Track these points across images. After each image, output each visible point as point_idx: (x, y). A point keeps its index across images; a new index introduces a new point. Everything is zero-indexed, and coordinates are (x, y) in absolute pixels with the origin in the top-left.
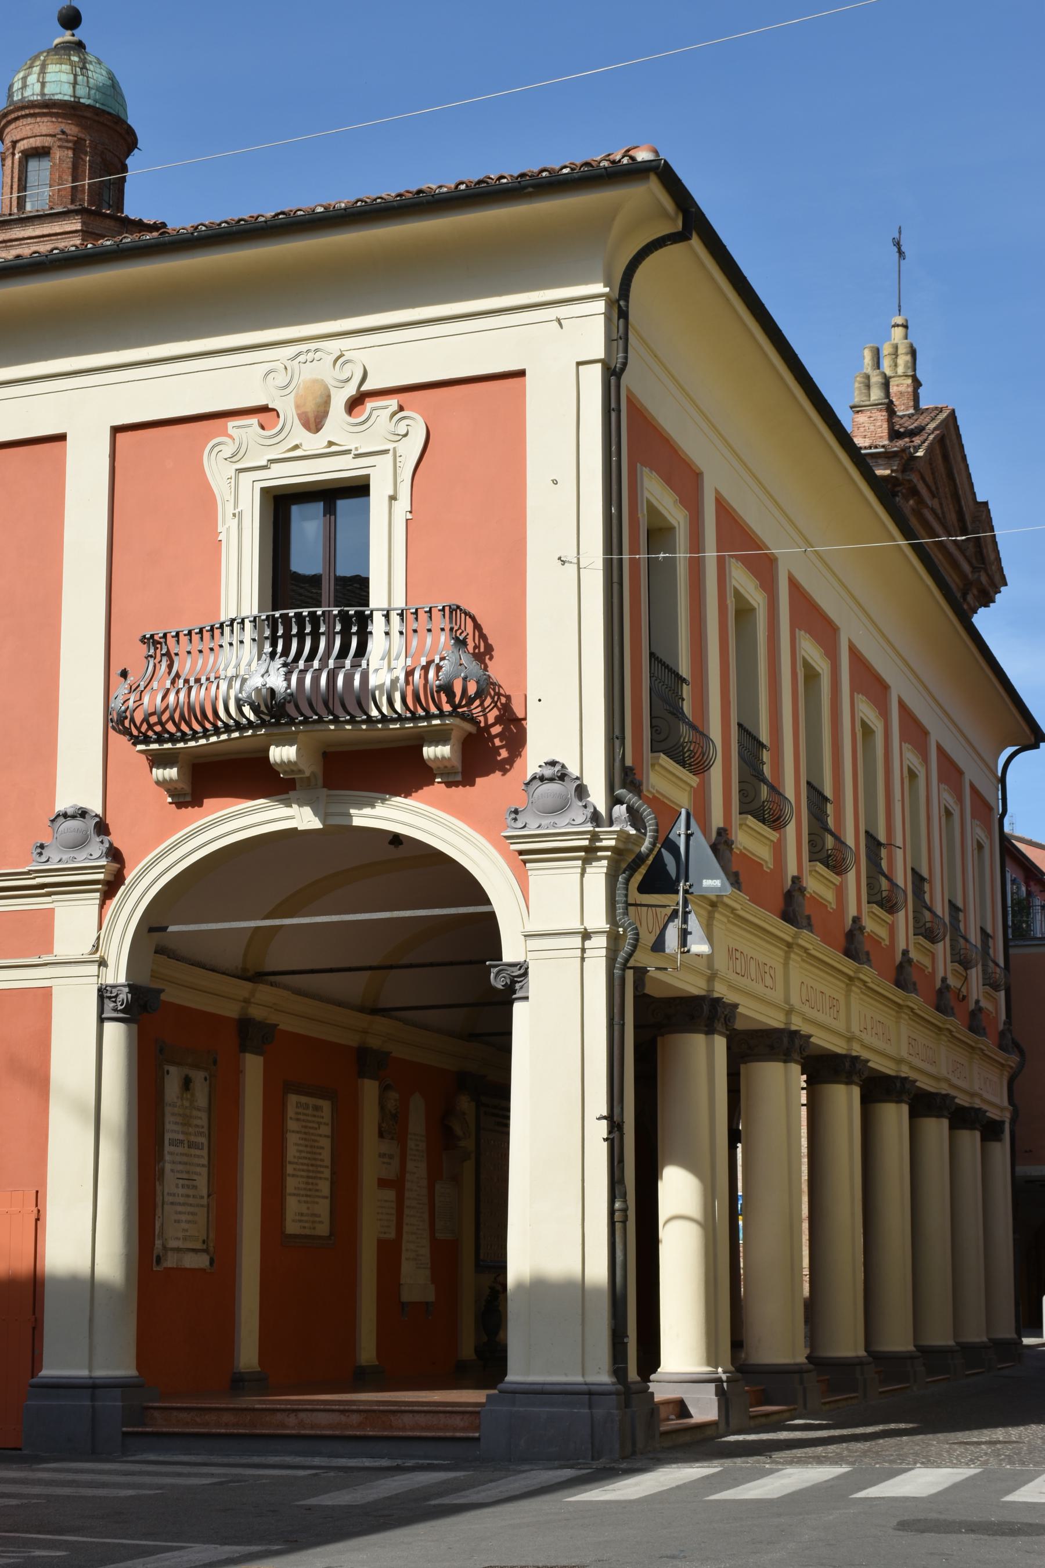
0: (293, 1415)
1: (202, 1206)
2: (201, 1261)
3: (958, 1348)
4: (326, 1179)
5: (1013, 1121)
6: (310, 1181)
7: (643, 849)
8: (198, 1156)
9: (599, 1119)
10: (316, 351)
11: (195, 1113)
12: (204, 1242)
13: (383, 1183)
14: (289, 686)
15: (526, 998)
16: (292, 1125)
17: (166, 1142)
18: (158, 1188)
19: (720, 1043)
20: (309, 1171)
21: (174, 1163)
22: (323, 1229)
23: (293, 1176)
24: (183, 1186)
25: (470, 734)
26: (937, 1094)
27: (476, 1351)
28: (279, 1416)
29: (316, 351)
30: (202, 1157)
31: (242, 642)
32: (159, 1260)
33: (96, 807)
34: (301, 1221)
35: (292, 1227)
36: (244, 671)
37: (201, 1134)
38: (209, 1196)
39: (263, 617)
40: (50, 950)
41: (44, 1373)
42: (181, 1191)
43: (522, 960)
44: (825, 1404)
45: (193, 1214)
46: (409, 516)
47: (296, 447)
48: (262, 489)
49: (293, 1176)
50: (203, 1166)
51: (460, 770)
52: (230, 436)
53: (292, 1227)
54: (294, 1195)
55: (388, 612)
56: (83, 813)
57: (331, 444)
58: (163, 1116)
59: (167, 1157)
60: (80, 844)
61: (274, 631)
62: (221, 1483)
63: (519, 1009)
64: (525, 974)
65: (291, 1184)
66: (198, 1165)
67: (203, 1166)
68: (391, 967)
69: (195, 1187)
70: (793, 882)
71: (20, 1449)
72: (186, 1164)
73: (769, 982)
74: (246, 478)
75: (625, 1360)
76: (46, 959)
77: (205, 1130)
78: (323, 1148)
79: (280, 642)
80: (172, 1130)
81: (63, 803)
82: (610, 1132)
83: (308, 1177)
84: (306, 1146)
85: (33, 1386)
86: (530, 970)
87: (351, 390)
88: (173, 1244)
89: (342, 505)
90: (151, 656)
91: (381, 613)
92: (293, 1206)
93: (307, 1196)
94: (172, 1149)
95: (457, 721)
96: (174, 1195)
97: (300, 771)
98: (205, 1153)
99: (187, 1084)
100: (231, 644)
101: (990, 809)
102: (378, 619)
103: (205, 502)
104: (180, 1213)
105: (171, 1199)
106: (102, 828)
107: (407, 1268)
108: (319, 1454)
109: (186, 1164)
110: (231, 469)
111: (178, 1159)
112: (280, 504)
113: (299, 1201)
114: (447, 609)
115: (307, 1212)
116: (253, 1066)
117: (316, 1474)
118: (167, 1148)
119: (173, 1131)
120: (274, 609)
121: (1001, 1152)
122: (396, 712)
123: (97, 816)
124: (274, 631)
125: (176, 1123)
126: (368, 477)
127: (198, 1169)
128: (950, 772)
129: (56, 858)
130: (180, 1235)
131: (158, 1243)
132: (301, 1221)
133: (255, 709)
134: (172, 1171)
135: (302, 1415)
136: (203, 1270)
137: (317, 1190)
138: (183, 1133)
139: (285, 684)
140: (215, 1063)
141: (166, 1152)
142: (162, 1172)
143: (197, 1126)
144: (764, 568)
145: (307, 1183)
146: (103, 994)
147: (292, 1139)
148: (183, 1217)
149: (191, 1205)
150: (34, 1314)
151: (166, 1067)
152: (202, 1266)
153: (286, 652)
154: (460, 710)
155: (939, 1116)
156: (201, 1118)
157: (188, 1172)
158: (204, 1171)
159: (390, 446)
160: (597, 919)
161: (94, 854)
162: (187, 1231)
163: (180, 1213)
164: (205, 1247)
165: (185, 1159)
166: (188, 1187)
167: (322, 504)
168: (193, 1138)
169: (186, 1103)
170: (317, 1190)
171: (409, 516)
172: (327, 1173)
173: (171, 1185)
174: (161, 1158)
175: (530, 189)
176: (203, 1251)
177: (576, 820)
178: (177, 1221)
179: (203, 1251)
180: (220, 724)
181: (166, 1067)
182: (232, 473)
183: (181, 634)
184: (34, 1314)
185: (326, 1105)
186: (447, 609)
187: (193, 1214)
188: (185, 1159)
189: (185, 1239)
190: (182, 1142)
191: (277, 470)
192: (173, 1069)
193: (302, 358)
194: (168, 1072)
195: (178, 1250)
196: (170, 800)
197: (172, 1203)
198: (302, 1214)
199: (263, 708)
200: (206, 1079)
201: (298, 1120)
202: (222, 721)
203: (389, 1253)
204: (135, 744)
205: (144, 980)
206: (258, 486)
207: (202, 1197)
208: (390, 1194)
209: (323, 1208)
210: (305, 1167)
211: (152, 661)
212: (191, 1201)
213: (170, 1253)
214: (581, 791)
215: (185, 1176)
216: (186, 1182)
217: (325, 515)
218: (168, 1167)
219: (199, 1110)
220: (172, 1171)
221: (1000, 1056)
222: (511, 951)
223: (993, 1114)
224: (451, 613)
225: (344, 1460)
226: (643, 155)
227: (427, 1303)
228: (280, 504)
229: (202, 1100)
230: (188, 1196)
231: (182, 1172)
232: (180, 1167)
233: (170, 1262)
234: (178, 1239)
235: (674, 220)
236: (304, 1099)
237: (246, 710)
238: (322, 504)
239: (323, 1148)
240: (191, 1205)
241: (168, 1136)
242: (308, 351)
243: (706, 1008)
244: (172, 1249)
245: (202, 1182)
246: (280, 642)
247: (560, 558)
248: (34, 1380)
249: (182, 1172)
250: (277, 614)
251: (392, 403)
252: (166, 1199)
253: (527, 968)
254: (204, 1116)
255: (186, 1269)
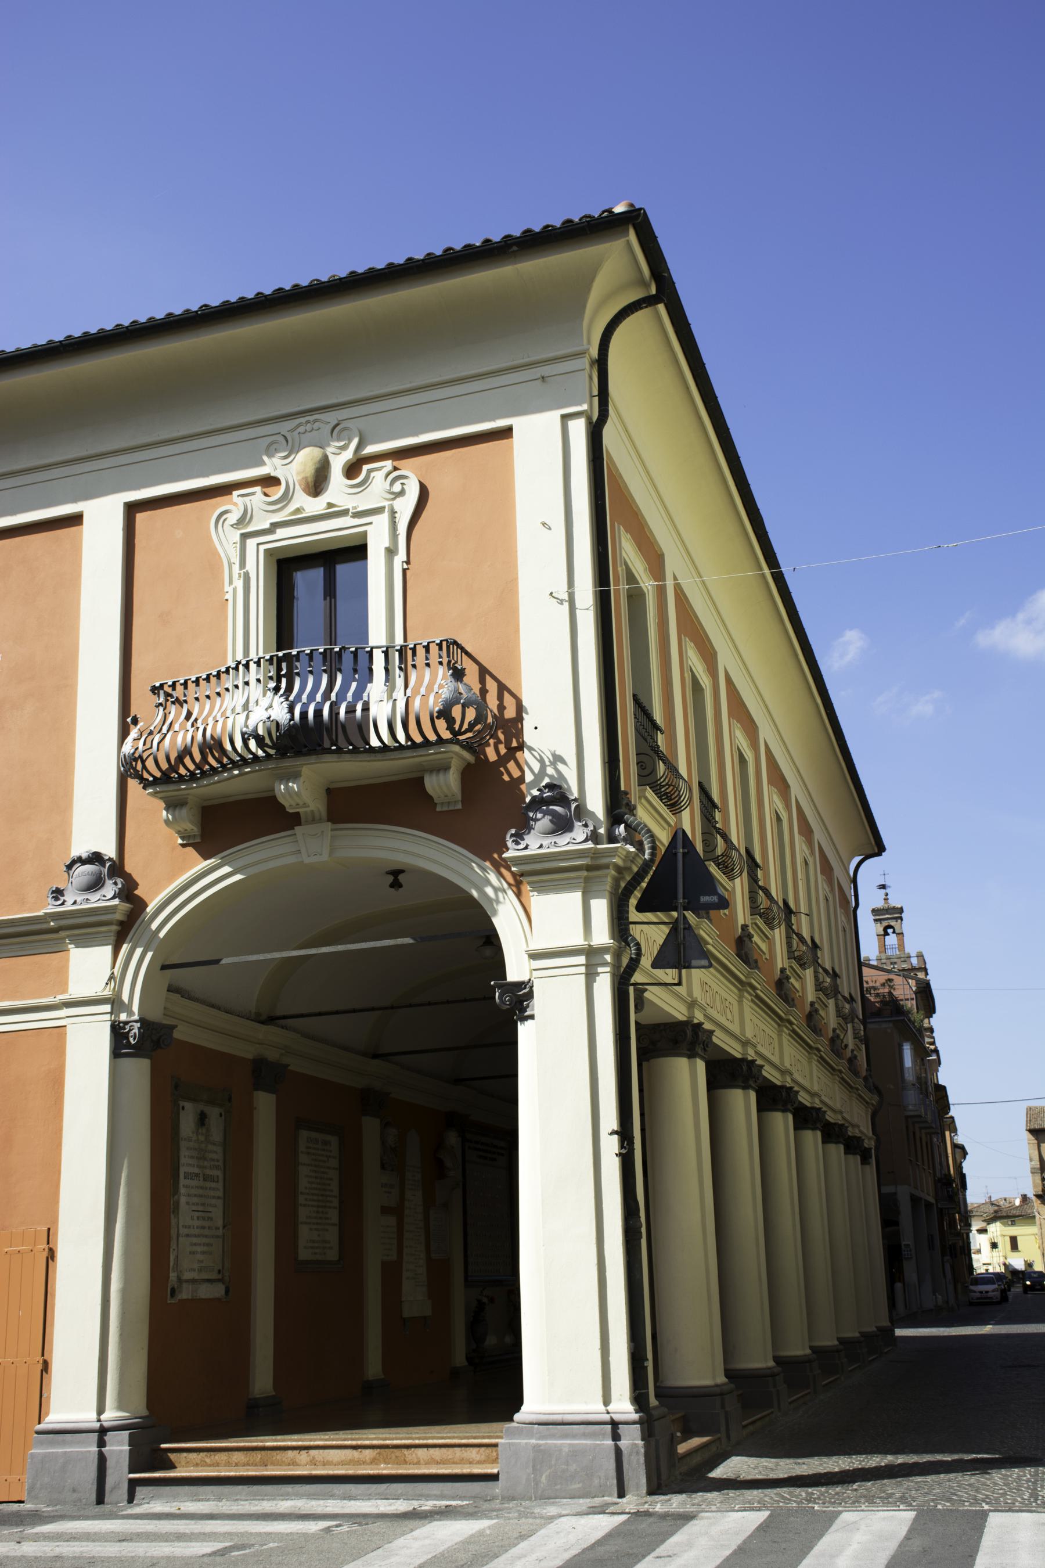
0: (304, 1452)
1: (218, 1237)
2: (216, 1291)
3: (862, 1339)
4: (335, 1208)
5: (877, 1148)
6: (320, 1210)
7: (647, 856)
8: (214, 1189)
9: (611, 1134)
10: (315, 421)
11: (210, 1147)
12: (219, 1272)
13: (385, 1210)
14: (292, 718)
15: (532, 1017)
16: (303, 1158)
17: (182, 1176)
18: (173, 1221)
19: (701, 1065)
20: (319, 1201)
21: (189, 1195)
22: (333, 1255)
23: (305, 1205)
24: (198, 1218)
25: (469, 764)
26: (835, 1124)
27: (468, 1359)
28: (290, 1454)
29: (315, 421)
30: (218, 1189)
31: (247, 683)
32: (173, 1292)
33: (109, 851)
34: (312, 1248)
35: (304, 1254)
36: (251, 709)
37: (217, 1167)
38: (224, 1227)
39: (268, 657)
40: (65, 991)
41: (48, 1419)
42: (196, 1223)
43: (526, 978)
44: (790, 1403)
45: (208, 1245)
46: (405, 566)
47: (298, 511)
48: (266, 550)
49: (305, 1205)
50: (219, 1198)
51: (459, 797)
52: (235, 504)
53: (304, 1254)
54: (306, 1223)
55: (387, 648)
56: (96, 858)
57: (330, 505)
58: (178, 1150)
59: (183, 1191)
60: (95, 885)
61: (279, 669)
62: (222, 1552)
63: (525, 1032)
64: (530, 995)
65: (303, 1213)
66: (214, 1197)
67: (219, 1198)
68: (392, 1007)
69: (210, 1219)
70: (742, 929)
71: (23, 1502)
72: (201, 1196)
73: (729, 1017)
74: (251, 543)
75: (646, 1386)
76: (61, 997)
77: (221, 1163)
78: (331, 1179)
79: (284, 681)
80: (187, 1163)
81: (80, 848)
82: (622, 1147)
83: (318, 1206)
84: (316, 1178)
85: (38, 1433)
86: (534, 989)
87: (348, 455)
88: (188, 1275)
89: (343, 570)
90: (161, 704)
91: (380, 650)
92: (305, 1233)
93: (317, 1224)
94: (188, 1182)
95: (456, 748)
96: (189, 1227)
97: (305, 805)
98: (220, 1185)
99: (202, 1119)
100: (237, 687)
101: (848, 902)
102: (379, 658)
103: (212, 564)
104: (195, 1244)
105: (185, 1231)
106: (117, 869)
107: (407, 1286)
108: (332, 1496)
109: (201, 1196)
110: (236, 535)
111: (193, 1191)
112: (286, 567)
113: (311, 1229)
114: (444, 643)
115: (317, 1240)
116: (265, 1104)
117: (328, 1530)
118: (182, 1181)
119: (189, 1165)
120: (278, 650)
121: (871, 1171)
122: (397, 741)
123: (110, 859)
124: (279, 669)
125: (192, 1157)
126: (365, 533)
127: (213, 1201)
128: (827, 868)
129: (74, 900)
130: (196, 1266)
131: (173, 1276)
132: (312, 1248)
133: (260, 741)
134: (188, 1203)
135: (312, 1452)
136: (219, 1299)
137: (327, 1219)
138: (198, 1166)
139: (288, 716)
140: (230, 1100)
141: (181, 1185)
142: (177, 1204)
143: (213, 1160)
144: (709, 656)
145: (318, 1212)
146: (118, 1031)
147: (304, 1171)
148: (199, 1249)
149: (206, 1236)
150: (43, 1355)
151: (182, 1103)
152: (217, 1295)
153: (289, 689)
154: (461, 738)
155: (837, 1143)
156: (216, 1152)
157: (203, 1204)
158: (220, 1203)
159: (386, 503)
160: (602, 935)
161: (106, 897)
162: (202, 1262)
163: (195, 1244)
164: (220, 1277)
165: (201, 1192)
166: (204, 1219)
167: (322, 569)
168: (208, 1172)
169: (202, 1138)
170: (327, 1219)
171: (405, 566)
172: (336, 1202)
173: (186, 1218)
174: (176, 1191)
175: (515, 248)
176: (219, 1280)
177: (576, 839)
178: (193, 1253)
179: (219, 1280)
180: (225, 760)
181: (182, 1103)
182: (237, 538)
183: (189, 682)
184: (43, 1355)
185: (334, 1140)
186: (444, 643)
187: (208, 1245)
188: (201, 1192)
189: (200, 1270)
190: (197, 1175)
191: (281, 533)
192: (188, 1105)
193: (301, 429)
194: (183, 1108)
195: (193, 1281)
196: (180, 841)
197: (187, 1235)
198: (313, 1241)
199: (267, 741)
200: (221, 1115)
201: (308, 1153)
202: (229, 758)
203: (392, 1273)
204: (144, 788)
205: (156, 1015)
206: (262, 548)
207: (218, 1228)
208: (392, 1220)
209: (332, 1235)
210: (315, 1198)
211: (161, 709)
212: (206, 1232)
213: (185, 1285)
214: (581, 812)
215: (201, 1208)
216: (200, 1214)
217: (325, 599)
218: (183, 1200)
219: (214, 1144)
220: (188, 1203)
221: (867, 1095)
222: (516, 970)
223: (866, 1144)
224: (448, 647)
225: (358, 1503)
226: (619, 209)
227: (425, 1317)
228: (286, 567)
229: (217, 1135)
230: (203, 1228)
231: (197, 1204)
232: (195, 1200)
233: (185, 1294)
234: (194, 1270)
235: (647, 286)
236: (314, 1135)
237: (252, 744)
238: (322, 569)
239: (331, 1179)
240: (206, 1236)
241: (183, 1170)
242: (308, 422)
243: (689, 1033)
244: (187, 1281)
245: (217, 1213)
246: (284, 681)
247: (551, 594)
248: (41, 1427)
249: (197, 1204)
250: (281, 654)
251: (388, 464)
252: (181, 1231)
253: (532, 987)
254: (219, 1149)
255: (201, 1300)
